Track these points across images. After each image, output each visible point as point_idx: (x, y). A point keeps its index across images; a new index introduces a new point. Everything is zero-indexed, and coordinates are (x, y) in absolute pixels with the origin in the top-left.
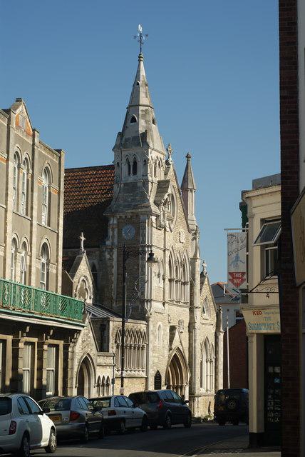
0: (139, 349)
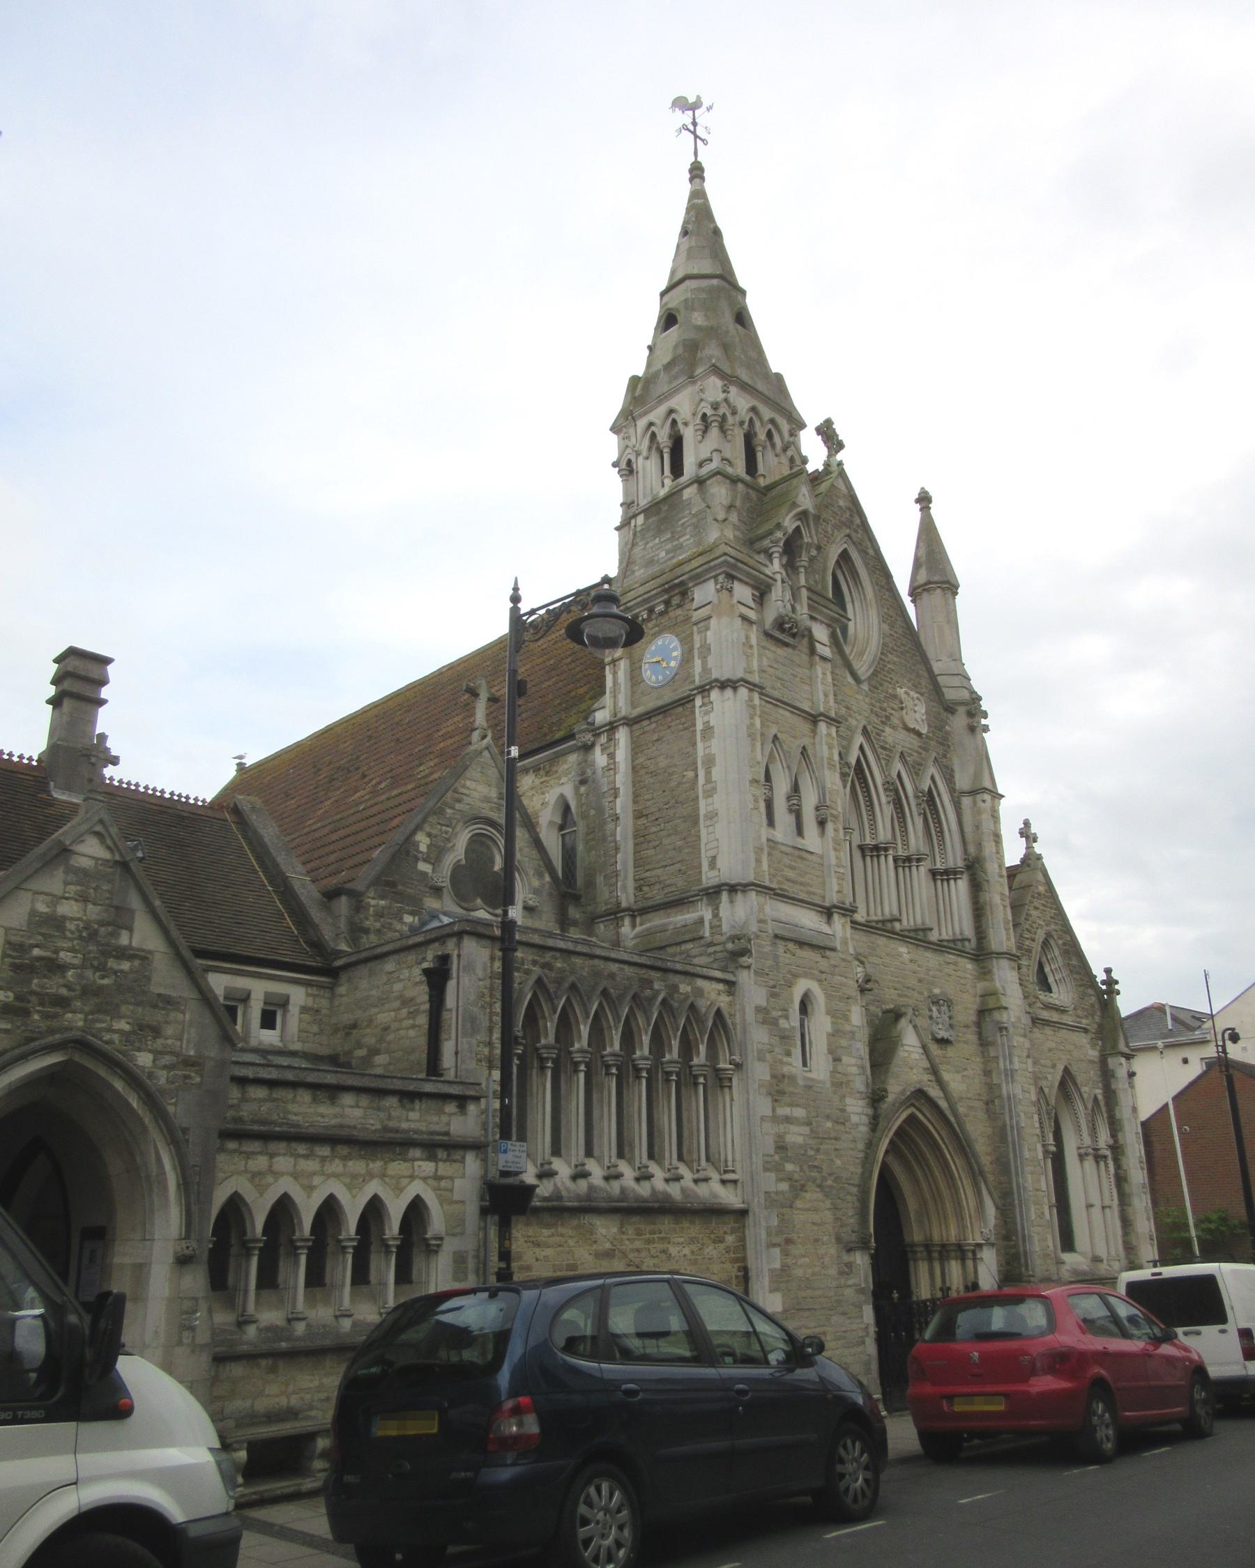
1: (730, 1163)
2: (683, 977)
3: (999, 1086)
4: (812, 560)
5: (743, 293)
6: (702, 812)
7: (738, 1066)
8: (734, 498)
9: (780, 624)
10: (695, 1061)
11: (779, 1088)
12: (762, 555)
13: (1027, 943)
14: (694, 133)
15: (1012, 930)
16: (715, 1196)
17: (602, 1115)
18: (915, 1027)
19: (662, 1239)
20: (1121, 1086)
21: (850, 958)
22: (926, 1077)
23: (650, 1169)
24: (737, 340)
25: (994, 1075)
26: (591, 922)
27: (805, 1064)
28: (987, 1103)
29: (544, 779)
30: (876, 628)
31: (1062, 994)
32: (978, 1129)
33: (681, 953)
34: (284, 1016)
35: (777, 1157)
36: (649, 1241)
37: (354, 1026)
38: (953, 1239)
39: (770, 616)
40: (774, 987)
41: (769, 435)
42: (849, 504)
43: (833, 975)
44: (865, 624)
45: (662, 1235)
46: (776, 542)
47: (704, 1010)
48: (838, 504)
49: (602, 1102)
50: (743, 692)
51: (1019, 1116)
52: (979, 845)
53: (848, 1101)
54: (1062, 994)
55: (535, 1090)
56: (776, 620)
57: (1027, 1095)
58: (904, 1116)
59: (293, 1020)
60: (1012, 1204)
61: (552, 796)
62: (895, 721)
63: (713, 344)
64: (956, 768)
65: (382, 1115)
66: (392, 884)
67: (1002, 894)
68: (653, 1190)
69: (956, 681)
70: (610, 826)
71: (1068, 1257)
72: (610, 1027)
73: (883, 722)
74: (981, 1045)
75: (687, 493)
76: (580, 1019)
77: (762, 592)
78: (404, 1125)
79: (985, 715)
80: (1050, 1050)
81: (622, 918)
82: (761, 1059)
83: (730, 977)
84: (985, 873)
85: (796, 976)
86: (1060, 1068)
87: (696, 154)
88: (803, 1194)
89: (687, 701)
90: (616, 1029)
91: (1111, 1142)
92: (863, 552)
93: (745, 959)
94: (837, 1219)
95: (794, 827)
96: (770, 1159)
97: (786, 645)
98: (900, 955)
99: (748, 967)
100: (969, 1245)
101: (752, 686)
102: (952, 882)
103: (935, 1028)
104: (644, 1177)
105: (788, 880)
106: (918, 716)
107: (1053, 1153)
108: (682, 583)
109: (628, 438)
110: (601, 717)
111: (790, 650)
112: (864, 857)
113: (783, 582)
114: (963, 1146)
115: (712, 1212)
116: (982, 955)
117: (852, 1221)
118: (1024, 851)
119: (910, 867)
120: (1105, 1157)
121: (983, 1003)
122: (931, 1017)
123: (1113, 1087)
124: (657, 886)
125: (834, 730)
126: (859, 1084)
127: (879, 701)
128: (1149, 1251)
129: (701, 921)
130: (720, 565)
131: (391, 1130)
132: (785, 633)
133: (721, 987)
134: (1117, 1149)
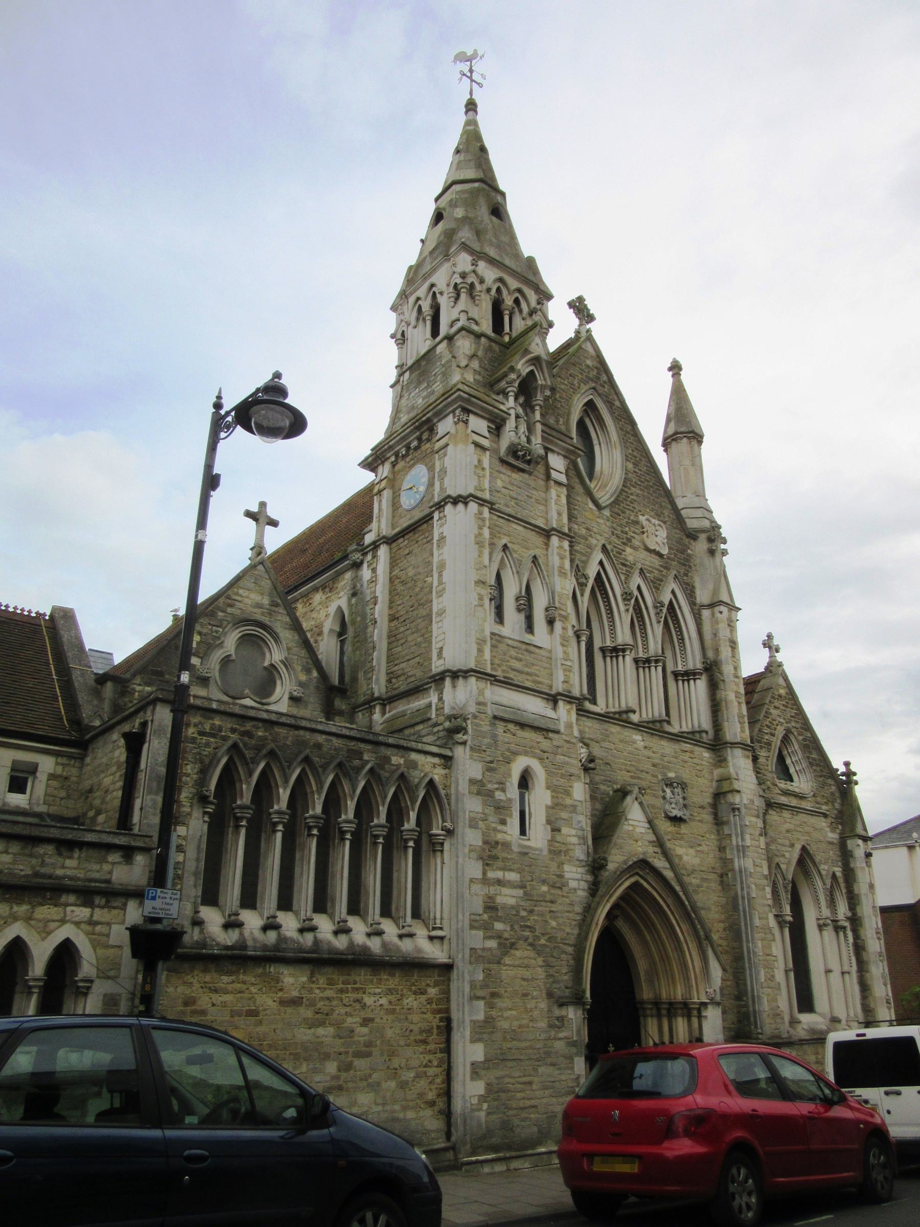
1: (438, 921)
2: (396, 751)
3: (732, 861)
4: (546, 399)
5: (503, 194)
6: (435, 610)
7: (450, 832)
8: (477, 350)
9: (514, 451)
10: (406, 826)
11: (492, 852)
12: (501, 396)
13: (767, 737)
14: (471, 78)
15: (746, 725)
16: (419, 950)
17: (429, 889)
18: (641, 804)
19: (357, 989)
20: (858, 865)
21: (574, 740)
22: (651, 849)
23: (278, 920)
24: (490, 227)
25: (728, 851)
26: (354, 709)
27: (523, 832)
28: (721, 876)
29: (329, 594)
30: (619, 465)
31: (803, 783)
32: (709, 901)
33: (414, 734)
34: (33, 782)
35: (485, 917)
36: (342, 991)
37: (91, 791)
38: (679, 998)
39: (504, 444)
40: (491, 762)
41: (517, 301)
42: (596, 364)
43: (556, 754)
44: (610, 462)
45: (358, 986)
46: (510, 383)
47: (417, 780)
48: (583, 362)
49: (303, 860)
50: (473, 506)
51: (749, 887)
52: (717, 651)
53: (566, 868)
54: (803, 783)
55: (229, 846)
56: (509, 448)
57: (758, 869)
58: (627, 884)
59: (39, 787)
60: (743, 968)
61: (332, 609)
62: (636, 543)
63: (466, 228)
64: (698, 585)
65: (34, 861)
66: (160, 674)
67: (737, 693)
68: (351, 943)
69: (699, 513)
70: (370, 629)
71: (806, 1019)
72: (313, 792)
73: (624, 543)
74: (717, 824)
75: (439, 349)
76: (279, 783)
77: (497, 425)
78: (59, 872)
80: (788, 831)
81: (374, 706)
82: (473, 824)
83: (448, 753)
84: (721, 673)
85: (515, 754)
86: (798, 847)
87: (471, 94)
88: (513, 952)
89: (428, 518)
90: (319, 794)
91: (849, 914)
92: (610, 404)
93: (460, 735)
94: (549, 976)
95: (524, 626)
96: (478, 918)
97: (522, 471)
98: (634, 742)
99: (464, 743)
100: (694, 1003)
101: (482, 502)
102: (692, 682)
103: (667, 807)
104: (342, 930)
105: (513, 670)
106: (658, 539)
107: (790, 923)
108: (429, 420)
109: (403, 313)
110: (369, 539)
111: (526, 476)
112: (604, 657)
113: (517, 417)
114: (690, 914)
115: (414, 966)
116: (718, 745)
117: (566, 978)
118: (767, 660)
119: (649, 668)
120: (844, 928)
121: (718, 787)
122: (664, 798)
123: (852, 866)
124: (402, 678)
125: (566, 544)
126: (579, 853)
127: (621, 525)
128: (885, 1012)
129: (429, 706)
130: (455, 400)
131: (44, 876)
132: (519, 460)
133: (436, 760)
134: (855, 921)
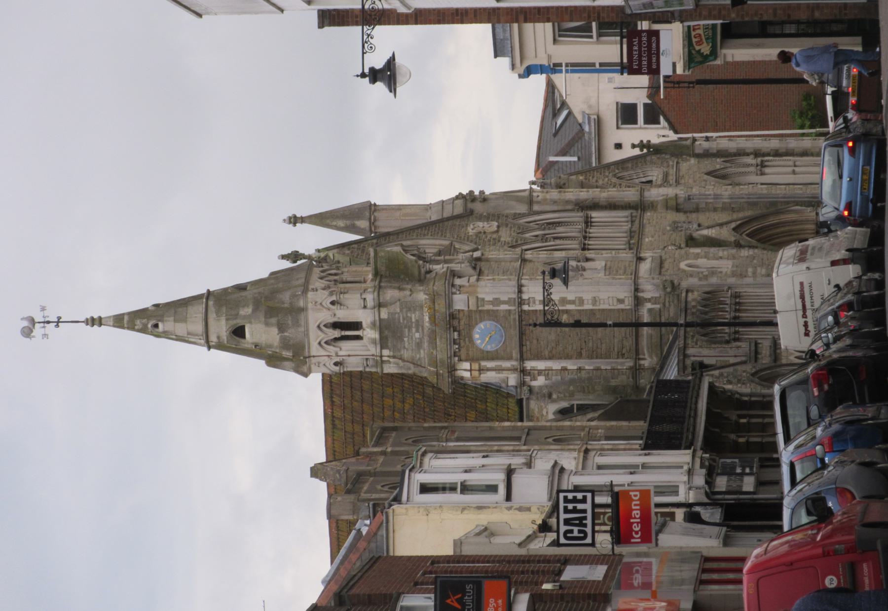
0: (739, 303)
3: (724, 203)
6: (590, 307)
50: (523, 282)
52: (568, 202)
79: (471, 192)
81: (640, 365)
84: (587, 200)
85: (679, 269)
91: (752, 156)
102: (593, 220)
120: (762, 161)
121: (672, 209)
123: (715, 151)
134: (757, 154)
